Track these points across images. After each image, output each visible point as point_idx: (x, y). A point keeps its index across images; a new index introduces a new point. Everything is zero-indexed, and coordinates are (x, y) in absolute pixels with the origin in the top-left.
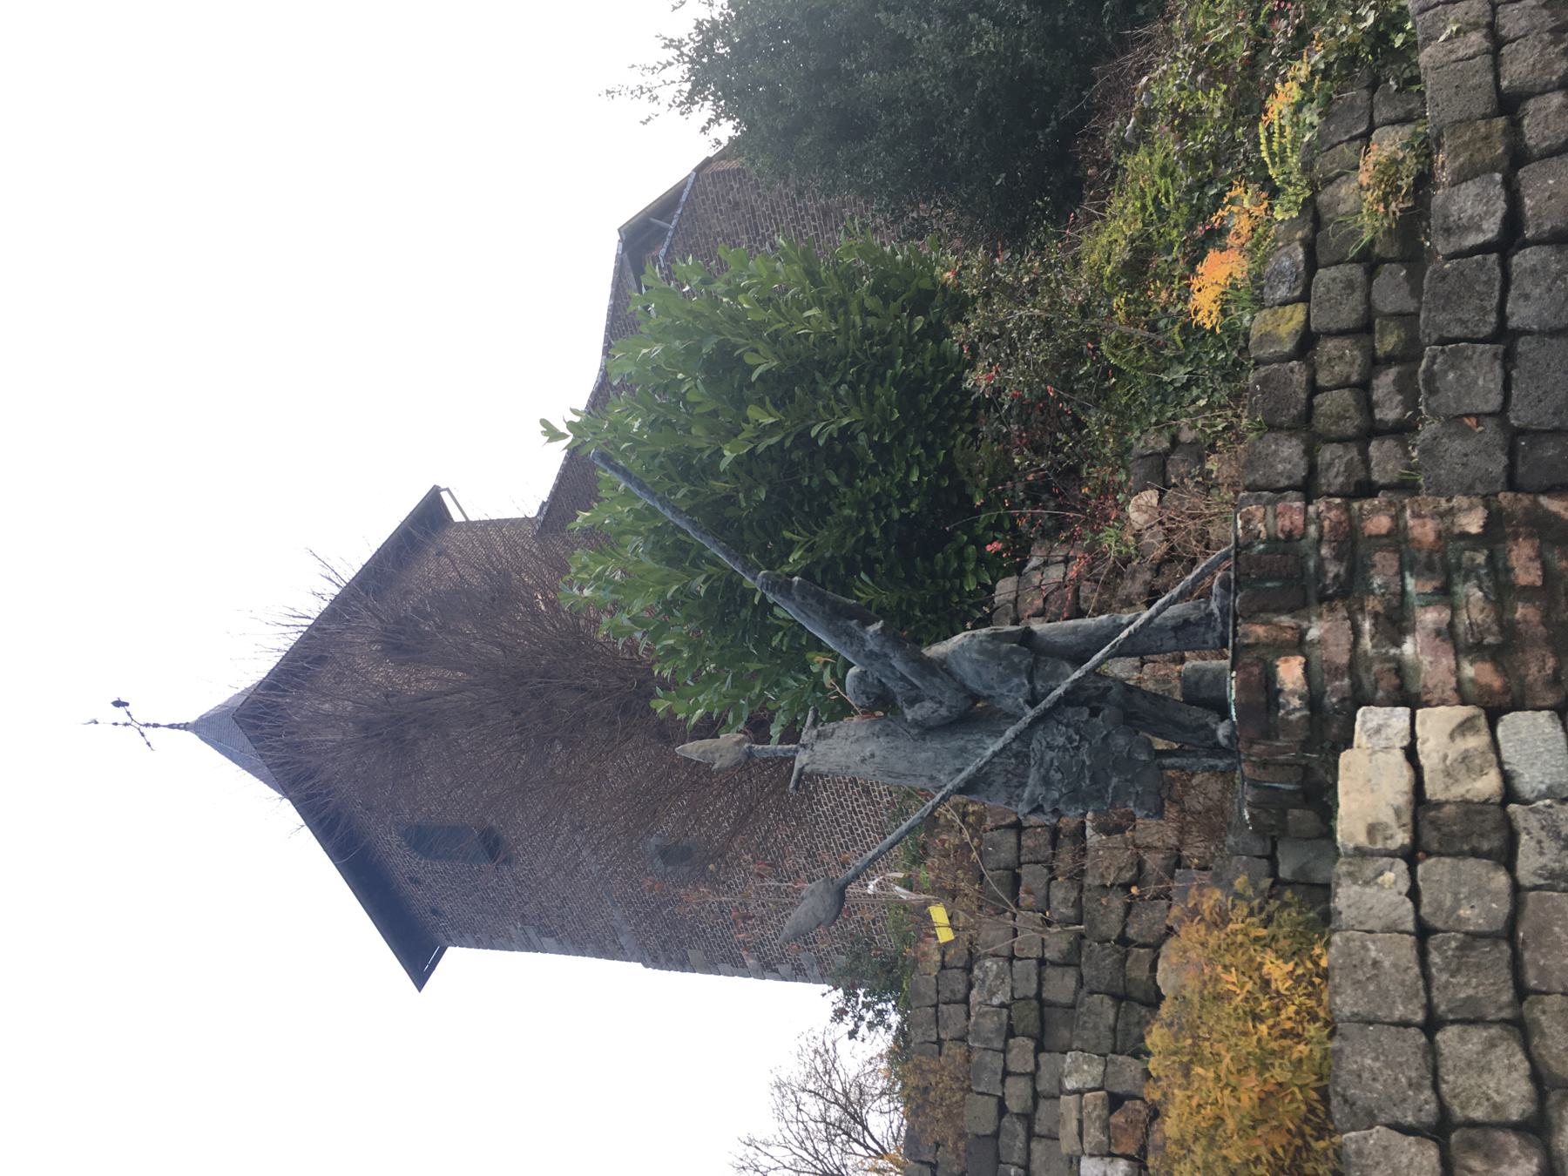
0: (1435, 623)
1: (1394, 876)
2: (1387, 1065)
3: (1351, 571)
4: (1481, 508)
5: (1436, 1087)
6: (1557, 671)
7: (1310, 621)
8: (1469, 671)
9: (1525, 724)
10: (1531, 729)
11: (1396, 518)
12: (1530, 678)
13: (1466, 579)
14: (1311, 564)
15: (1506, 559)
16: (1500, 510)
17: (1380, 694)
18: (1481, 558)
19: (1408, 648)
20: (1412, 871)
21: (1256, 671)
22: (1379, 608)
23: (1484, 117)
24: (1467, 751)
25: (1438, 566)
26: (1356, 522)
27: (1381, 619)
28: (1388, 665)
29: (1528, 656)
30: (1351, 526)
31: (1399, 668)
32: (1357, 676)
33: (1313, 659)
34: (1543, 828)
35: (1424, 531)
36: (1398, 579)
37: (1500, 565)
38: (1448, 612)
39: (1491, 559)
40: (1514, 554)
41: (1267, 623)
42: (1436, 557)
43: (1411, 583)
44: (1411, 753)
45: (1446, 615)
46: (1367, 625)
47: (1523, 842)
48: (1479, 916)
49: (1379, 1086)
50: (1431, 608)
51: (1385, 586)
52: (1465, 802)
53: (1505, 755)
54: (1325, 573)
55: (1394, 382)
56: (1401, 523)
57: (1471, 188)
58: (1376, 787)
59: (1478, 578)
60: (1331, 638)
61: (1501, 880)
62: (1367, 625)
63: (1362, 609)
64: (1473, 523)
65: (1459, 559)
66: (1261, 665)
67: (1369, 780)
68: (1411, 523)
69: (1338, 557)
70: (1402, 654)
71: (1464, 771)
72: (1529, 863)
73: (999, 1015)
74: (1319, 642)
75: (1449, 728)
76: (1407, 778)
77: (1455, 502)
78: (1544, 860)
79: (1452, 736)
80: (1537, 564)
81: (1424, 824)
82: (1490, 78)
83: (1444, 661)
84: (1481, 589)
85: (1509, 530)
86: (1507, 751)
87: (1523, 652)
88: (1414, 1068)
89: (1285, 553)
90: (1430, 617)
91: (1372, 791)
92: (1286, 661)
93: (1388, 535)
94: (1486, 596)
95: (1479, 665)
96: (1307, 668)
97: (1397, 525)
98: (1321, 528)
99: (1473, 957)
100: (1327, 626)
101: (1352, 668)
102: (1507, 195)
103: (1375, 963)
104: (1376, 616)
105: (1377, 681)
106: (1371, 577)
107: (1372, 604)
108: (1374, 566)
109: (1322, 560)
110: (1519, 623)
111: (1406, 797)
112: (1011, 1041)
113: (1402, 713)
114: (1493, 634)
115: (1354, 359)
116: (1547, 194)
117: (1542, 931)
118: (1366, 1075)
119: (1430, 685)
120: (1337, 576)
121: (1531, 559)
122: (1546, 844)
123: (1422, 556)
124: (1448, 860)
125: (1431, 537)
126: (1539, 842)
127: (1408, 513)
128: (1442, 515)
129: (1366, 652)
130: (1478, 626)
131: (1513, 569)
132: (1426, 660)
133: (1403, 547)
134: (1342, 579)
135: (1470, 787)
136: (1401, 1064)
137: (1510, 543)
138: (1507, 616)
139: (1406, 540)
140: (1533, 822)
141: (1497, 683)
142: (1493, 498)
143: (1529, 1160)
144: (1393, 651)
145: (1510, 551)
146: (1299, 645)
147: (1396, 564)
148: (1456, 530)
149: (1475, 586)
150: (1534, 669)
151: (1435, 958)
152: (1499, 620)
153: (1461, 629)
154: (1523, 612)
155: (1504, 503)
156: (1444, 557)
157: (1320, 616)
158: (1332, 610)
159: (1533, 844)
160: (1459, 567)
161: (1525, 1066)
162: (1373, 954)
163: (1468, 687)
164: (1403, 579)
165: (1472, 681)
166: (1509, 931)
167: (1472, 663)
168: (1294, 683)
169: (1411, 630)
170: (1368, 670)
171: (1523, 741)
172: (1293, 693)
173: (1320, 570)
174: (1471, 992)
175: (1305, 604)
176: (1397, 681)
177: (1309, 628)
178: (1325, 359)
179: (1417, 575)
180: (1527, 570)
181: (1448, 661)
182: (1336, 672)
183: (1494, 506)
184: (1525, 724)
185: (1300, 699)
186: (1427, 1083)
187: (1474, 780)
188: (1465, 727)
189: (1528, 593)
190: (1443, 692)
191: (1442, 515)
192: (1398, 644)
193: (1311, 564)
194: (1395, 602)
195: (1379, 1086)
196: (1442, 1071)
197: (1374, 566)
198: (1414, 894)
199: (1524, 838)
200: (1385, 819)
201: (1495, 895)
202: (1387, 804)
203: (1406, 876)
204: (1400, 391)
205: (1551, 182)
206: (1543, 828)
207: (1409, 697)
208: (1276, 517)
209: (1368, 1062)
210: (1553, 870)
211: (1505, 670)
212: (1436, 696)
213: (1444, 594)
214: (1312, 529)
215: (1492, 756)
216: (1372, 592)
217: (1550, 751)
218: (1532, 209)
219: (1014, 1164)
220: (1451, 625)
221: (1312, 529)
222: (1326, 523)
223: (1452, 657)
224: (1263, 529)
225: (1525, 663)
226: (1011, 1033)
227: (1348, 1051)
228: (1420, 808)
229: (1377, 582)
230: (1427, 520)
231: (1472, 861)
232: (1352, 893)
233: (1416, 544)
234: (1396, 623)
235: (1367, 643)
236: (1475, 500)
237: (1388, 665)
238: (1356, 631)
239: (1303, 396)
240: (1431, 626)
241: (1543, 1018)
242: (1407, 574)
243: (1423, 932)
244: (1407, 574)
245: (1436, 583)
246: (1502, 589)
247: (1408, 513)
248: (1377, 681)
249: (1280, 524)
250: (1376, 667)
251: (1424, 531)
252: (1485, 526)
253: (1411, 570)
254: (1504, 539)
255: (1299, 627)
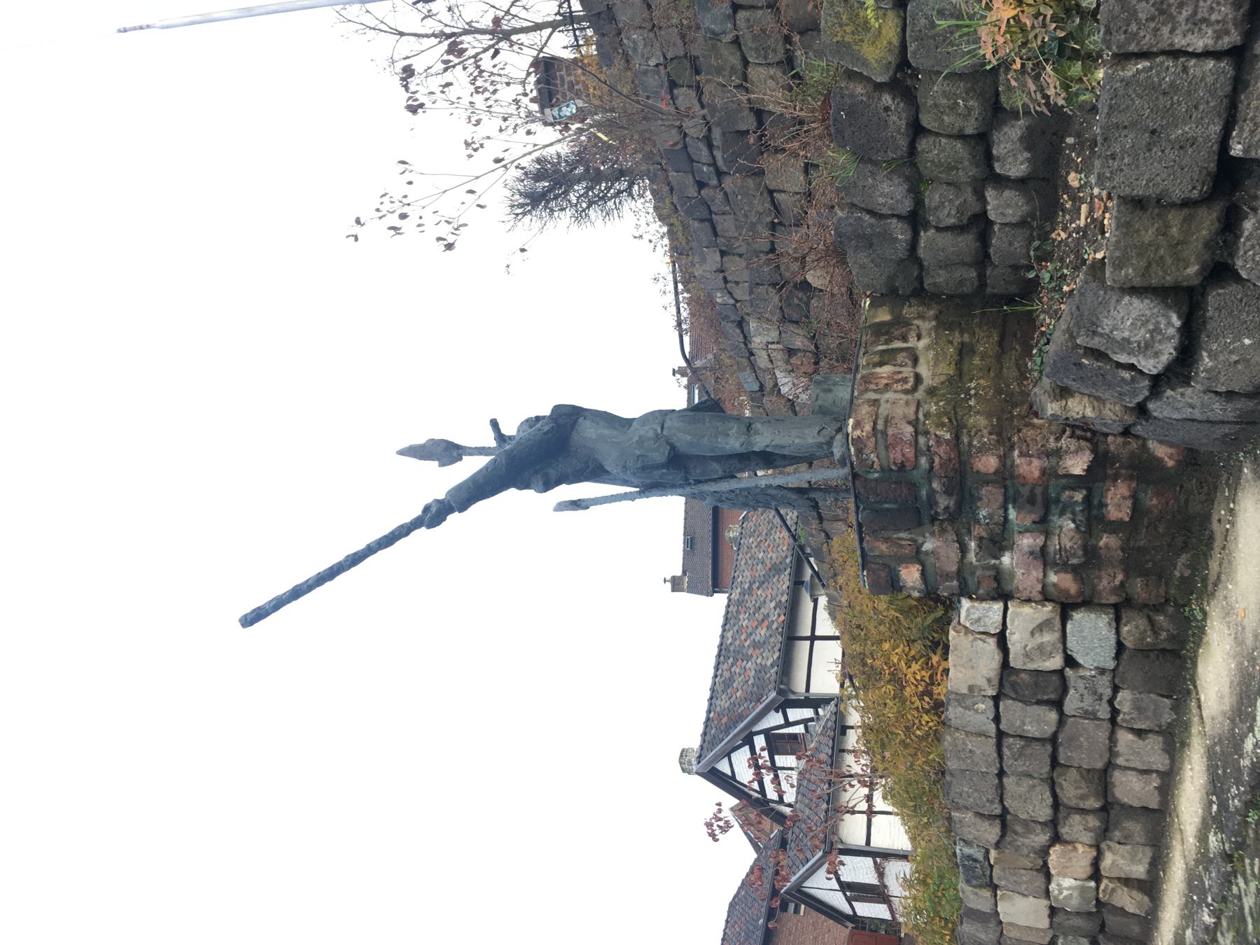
0: (1029, 546)
1: (985, 706)
2: (976, 791)
3: (960, 505)
4: (1088, 452)
5: (1001, 801)
6: (1122, 584)
7: (924, 537)
8: (1053, 578)
9: (1089, 625)
10: (1092, 630)
11: (1003, 459)
12: (1101, 587)
13: (1062, 513)
14: (924, 493)
15: (1102, 496)
16: (1107, 452)
17: (981, 591)
18: (1079, 496)
19: (1006, 559)
20: (997, 707)
21: (883, 574)
22: (984, 534)
23: (1186, 204)
24: (1042, 643)
25: (1039, 498)
26: (964, 458)
27: (984, 541)
28: (988, 573)
29: (1103, 573)
30: (960, 462)
31: (998, 576)
32: (964, 579)
33: (928, 567)
34: (1086, 688)
35: (1029, 468)
36: (1001, 512)
37: (1095, 502)
38: (1043, 538)
39: (1087, 500)
40: (1110, 494)
41: (886, 540)
42: (1039, 491)
43: (1012, 514)
44: (1001, 640)
45: (1040, 541)
46: (973, 545)
47: (1071, 693)
48: (1037, 731)
49: (971, 800)
50: (1028, 535)
51: (991, 516)
52: (1038, 672)
53: (1069, 645)
54: (936, 503)
55: (1021, 139)
56: (1009, 463)
57: (1138, 307)
58: (975, 665)
59: (1074, 513)
60: (942, 552)
61: (1053, 716)
62: (973, 545)
63: (969, 532)
64: (1077, 465)
65: (1059, 494)
66: (887, 570)
67: (971, 660)
68: (1018, 461)
69: (948, 492)
70: (1001, 563)
71: (1038, 654)
72: (1071, 705)
73: (658, 73)
74: (932, 552)
75: (1031, 627)
76: (997, 660)
77: (1064, 442)
78: (1081, 705)
79: (1032, 634)
80: (1129, 503)
81: (1007, 685)
82: (1215, 129)
83: (1034, 574)
84: (1074, 521)
85: (1109, 472)
86: (1072, 643)
87: (1100, 570)
88: (991, 794)
89: (898, 483)
90: (1027, 542)
91: (973, 668)
92: (906, 568)
93: (996, 472)
94: (1077, 527)
95: (1063, 575)
96: (923, 573)
97: (1004, 466)
98: (932, 462)
99: (1029, 751)
100: (939, 544)
101: (959, 573)
102: (1181, 343)
103: (971, 751)
104: (981, 539)
105: (979, 582)
106: (978, 508)
107: (978, 531)
108: (980, 499)
109: (932, 492)
110: (1101, 548)
111: (995, 672)
112: (675, 91)
113: (998, 607)
114: (1078, 558)
115: (969, 110)
116: (1234, 358)
117: (1072, 739)
118: (964, 795)
119: (1021, 588)
120: (947, 508)
121: (1124, 498)
122: (1086, 696)
123: (1025, 491)
124: (1020, 704)
125: (1037, 474)
126: (1082, 695)
127: (1016, 453)
128: (1048, 454)
129: (971, 563)
130: (1066, 551)
131: (1107, 505)
132: (1019, 572)
133: (1008, 483)
134: (951, 510)
135: (1041, 664)
136: (983, 792)
137: (1109, 483)
138: (1093, 541)
139: (1012, 477)
140: (1081, 684)
141: (1073, 591)
142: (1102, 439)
143: (1045, 834)
144: (993, 562)
145: (1109, 490)
146: (917, 556)
147: (1001, 499)
148: (1061, 472)
149: (1070, 519)
150: (1105, 582)
151: (1006, 751)
152: (1085, 548)
153: (1051, 550)
154: (1107, 541)
155: (1112, 447)
156: (1046, 488)
157: (933, 534)
158: (943, 531)
159: (1077, 695)
160: (1058, 501)
161: (1050, 801)
162: (970, 747)
163: (1051, 589)
164: (1006, 510)
165: (1055, 585)
166: (1053, 740)
167: (1056, 573)
168: (914, 582)
169: (1011, 548)
170: (973, 574)
171: (1084, 638)
172: (914, 588)
173: (932, 502)
174: (1025, 768)
175: (920, 524)
176: (996, 585)
177: (923, 543)
178: (930, 102)
179: (1019, 509)
180: (1118, 506)
181: (1037, 573)
182: (947, 577)
183: (1102, 447)
184: (1089, 625)
185: (919, 592)
186: (997, 801)
187: (1044, 661)
188: (1041, 628)
189: (1114, 527)
190: (1031, 592)
191: (1048, 454)
192: (997, 558)
193: (924, 493)
194: (997, 530)
195: (971, 800)
196: (1005, 796)
197: (980, 499)
198: (997, 719)
199: (1072, 692)
200: (978, 683)
201: (1047, 723)
202: (982, 677)
203: (993, 709)
204: (1028, 149)
205: (1247, 342)
206: (1086, 688)
207: (1002, 593)
208: (887, 448)
209: (966, 789)
210: (1087, 710)
211: (1082, 579)
212: (1024, 596)
213: (1043, 525)
214: (923, 461)
215: (1060, 646)
216: (978, 522)
217: (1102, 647)
218: (1206, 370)
219: (704, 164)
220: (1043, 549)
221: (923, 461)
222: (937, 460)
223: (1041, 570)
224: (875, 459)
225: (1100, 578)
226: (673, 85)
227: (954, 782)
228: (1006, 672)
229: (983, 513)
230: (1033, 459)
231: (1035, 707)
232: (957, 711)
233: (1021, 480)
234: (998, 542)
235: (972, 557)
236: (1083, 443)
237: (988, 573)
238: (963, 550)
239: (903, 142)
240: (1026, 549)
241: (1064, 783)
242: (1010, 506)
243: (1001, 735)
244: (1010, 506)
245: (1035, 517)
246: (1093, 519)
247: (1016, 453)
248: (979, 582)
249: (892, 456)
250: (978, 573)
251: (1029, 468)
252: (1089, 470)
253: (1014, 502)
254: (1105, 478)
255: (915, 541)
